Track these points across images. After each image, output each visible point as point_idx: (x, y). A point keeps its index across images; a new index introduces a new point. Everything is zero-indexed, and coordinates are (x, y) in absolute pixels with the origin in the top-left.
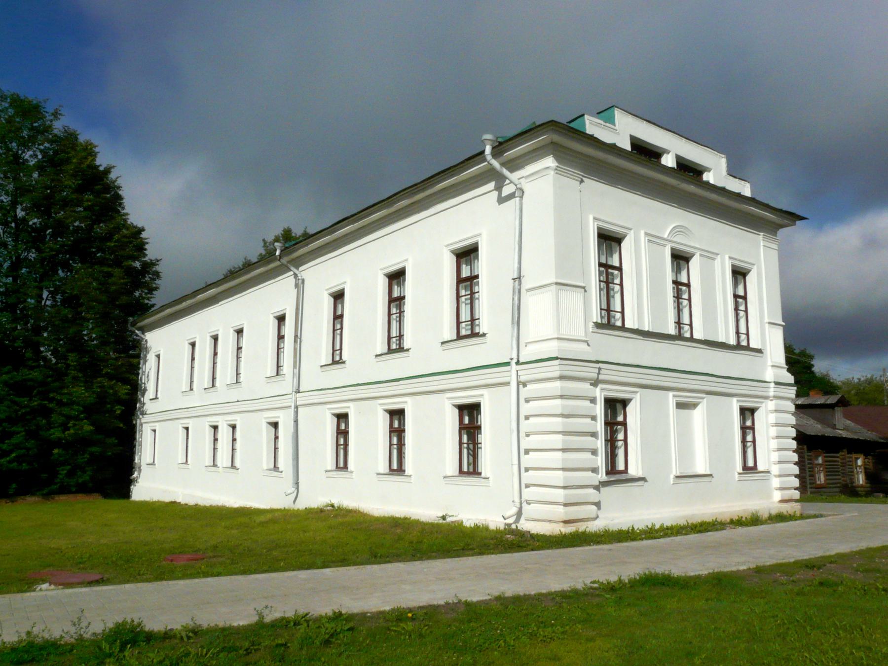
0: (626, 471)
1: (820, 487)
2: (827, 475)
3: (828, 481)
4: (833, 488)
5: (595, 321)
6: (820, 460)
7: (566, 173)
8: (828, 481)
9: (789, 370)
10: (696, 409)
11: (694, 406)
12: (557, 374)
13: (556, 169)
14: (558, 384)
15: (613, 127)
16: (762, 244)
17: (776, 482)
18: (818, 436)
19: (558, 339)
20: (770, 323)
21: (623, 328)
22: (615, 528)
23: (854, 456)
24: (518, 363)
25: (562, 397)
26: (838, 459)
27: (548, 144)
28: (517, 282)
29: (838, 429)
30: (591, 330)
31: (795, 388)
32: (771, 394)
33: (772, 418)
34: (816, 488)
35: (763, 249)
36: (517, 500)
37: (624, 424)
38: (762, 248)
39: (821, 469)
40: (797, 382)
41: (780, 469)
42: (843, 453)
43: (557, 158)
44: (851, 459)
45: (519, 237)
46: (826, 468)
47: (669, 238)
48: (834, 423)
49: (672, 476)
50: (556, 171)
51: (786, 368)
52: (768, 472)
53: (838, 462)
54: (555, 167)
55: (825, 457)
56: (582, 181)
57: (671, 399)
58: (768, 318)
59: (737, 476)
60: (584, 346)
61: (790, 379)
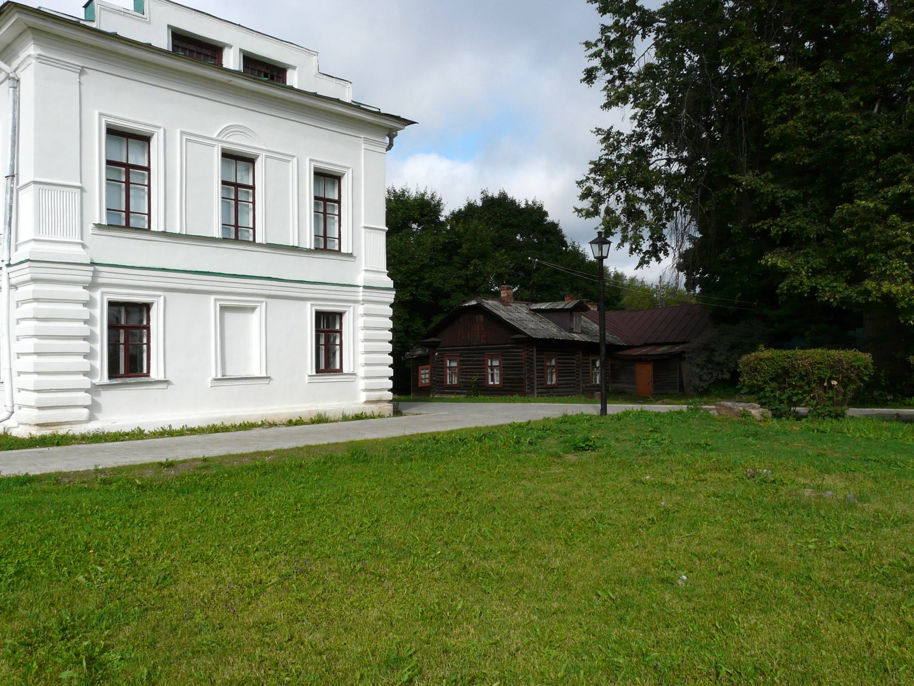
0: (148, 374)
1: (552, 387)
2: (559, 376)
3: (560, 382)
4: (565, 388)
5: (97, 222)
6: (553, 363)
7: (57, 63)
8: (560, 382)
9: (389, 275)
10: (255, 313)
11: (253, 309)
12: (27, 277)
13: (38, 58)
14: (32, 287)
15: (141, 15)
16: (363, 147)
17: (362, 384)
18: (546, 339)
19: (35, 240)
20: (365, 227)
21: (148, 231)
22: (113, 431)
23: (591, 358)
24: (9, 265)
25: (36, 300)
26: (574, 361)
27: (25, 31)
28: (9, 180)
29: (575, 333)
30: (91, 232)
31: (395, 292)
32: (360, 298)
33: (361, 322)
34: (546, 388)
35: (364, 151)
36: (9, 404)
37: (148, 328)
38: (363, 151)
39: (554, 370)
40: (396, 286)
41: (366, 372)
42: (578, 356)
43: (38, 42)
44: (588, 361)
45: (12, 132)
46: (559, 370)
47: (220, 138)
48: (572, 327)
49: (210, 379)
50: (39, 60)
51: (386, 272)
52: (354, 374)
53: (573, 363)
54: (36, 56)
55: (558, 359)
56: (82, 71)
57: (211, 304)
58: (365, 223)
59: (307, 378)
60: (79, 249)
61: (390, 283)
